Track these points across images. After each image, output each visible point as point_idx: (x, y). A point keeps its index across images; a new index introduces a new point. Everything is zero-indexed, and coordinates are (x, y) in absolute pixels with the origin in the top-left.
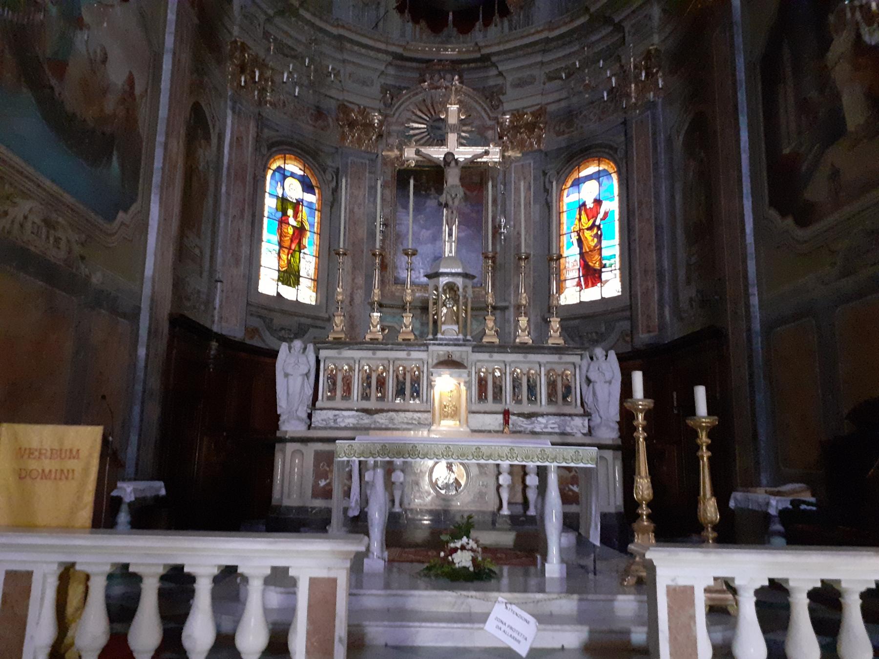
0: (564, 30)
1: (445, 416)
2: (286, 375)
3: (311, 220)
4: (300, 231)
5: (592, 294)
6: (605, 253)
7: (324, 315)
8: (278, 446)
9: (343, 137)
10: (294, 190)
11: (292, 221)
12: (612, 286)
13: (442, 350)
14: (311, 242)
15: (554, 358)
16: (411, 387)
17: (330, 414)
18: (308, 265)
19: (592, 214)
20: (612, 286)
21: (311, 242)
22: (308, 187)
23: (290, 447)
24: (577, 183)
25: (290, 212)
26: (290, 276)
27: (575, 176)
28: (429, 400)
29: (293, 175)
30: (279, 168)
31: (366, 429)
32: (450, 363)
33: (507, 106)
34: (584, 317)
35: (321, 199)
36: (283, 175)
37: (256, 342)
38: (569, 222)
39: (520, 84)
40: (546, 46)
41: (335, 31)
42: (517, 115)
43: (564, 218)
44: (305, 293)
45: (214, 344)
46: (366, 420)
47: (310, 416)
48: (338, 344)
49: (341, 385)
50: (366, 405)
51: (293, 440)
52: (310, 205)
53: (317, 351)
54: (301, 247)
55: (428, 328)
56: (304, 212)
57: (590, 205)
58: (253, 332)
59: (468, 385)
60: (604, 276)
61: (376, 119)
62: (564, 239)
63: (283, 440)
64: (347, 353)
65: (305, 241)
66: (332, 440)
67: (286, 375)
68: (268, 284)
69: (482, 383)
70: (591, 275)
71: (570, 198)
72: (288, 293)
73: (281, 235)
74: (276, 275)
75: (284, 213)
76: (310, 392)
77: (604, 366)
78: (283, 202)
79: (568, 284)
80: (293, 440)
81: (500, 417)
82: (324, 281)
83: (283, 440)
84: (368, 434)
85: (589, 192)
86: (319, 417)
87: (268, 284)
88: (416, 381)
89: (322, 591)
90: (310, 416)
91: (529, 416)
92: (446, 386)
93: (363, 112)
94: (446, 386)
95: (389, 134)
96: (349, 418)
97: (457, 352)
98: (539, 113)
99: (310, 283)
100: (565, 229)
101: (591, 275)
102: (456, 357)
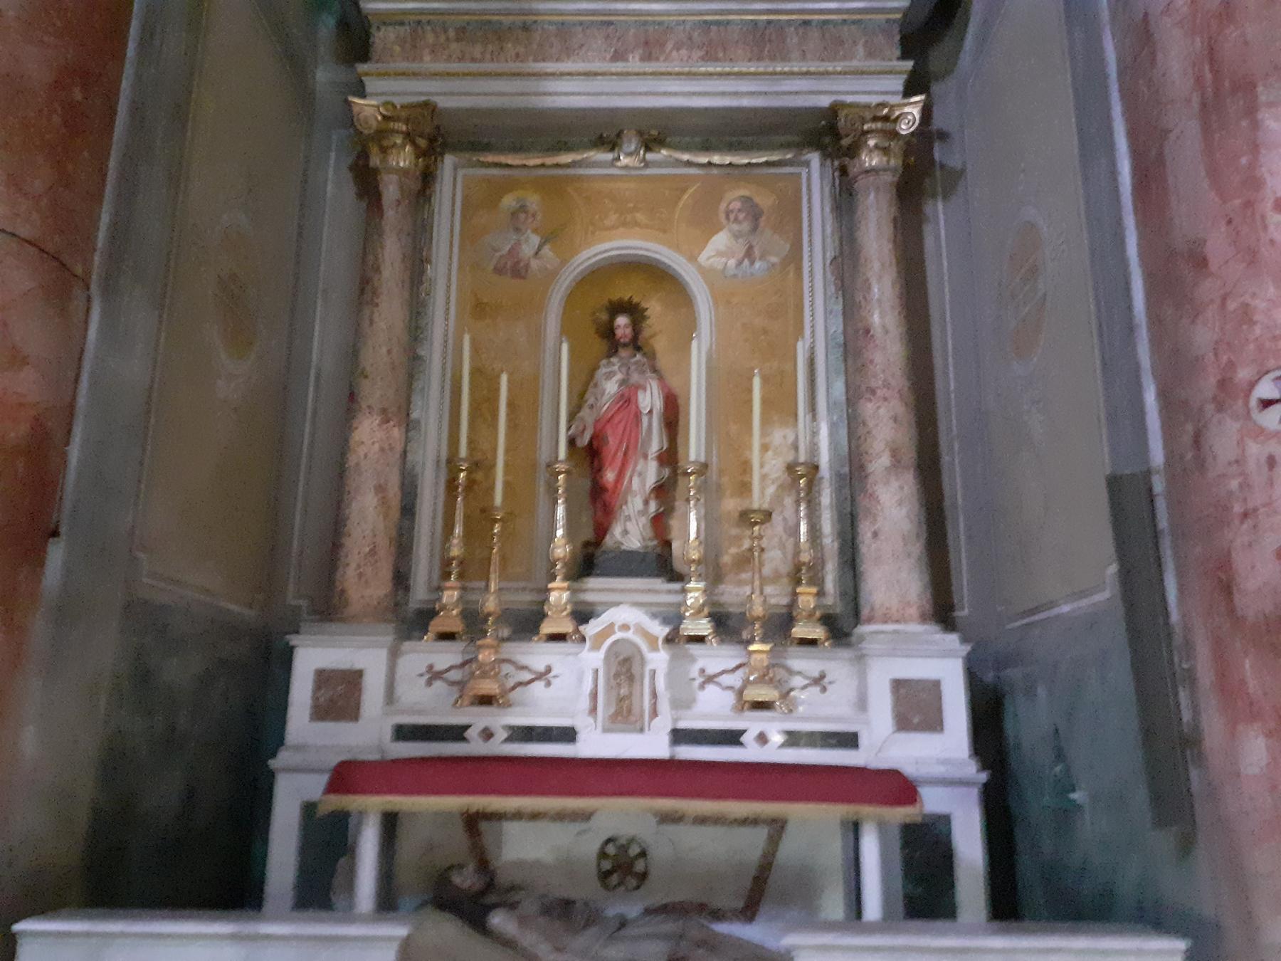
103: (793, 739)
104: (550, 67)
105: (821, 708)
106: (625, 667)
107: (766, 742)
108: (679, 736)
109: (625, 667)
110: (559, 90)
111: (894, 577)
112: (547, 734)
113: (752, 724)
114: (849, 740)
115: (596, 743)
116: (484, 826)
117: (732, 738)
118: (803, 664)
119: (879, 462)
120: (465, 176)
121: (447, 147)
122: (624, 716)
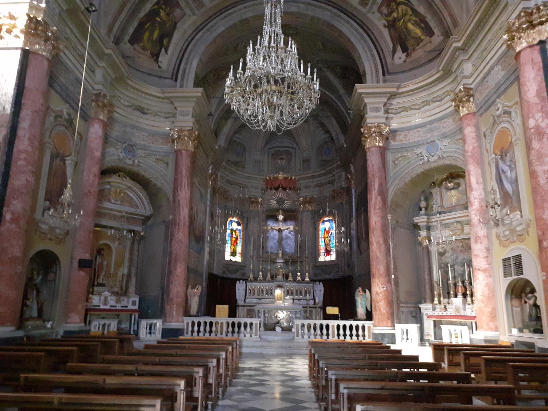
0: (318, 173)
1: (278, 300)
2: (239, 289)
3: (240, 235)
4: (237, 239)
5: (328, 258)
6: (331, 246)
7: (244, 265)
8: (237, 308)
9: (250, 207)
10: (235, 226)
11: (234, 236)
12: (333, 257)
13: (277, 283)
14: (240, 242)
15: (306, 285)
16: (270, 292)
17: (250, 299)
18: (239, 249)
19: (328, 232)
20: (333, 257)
21: (240, 242)
22: (239, 224)
23: (240, 308)
24: (324, 222)
25: (234, 233)
26: (234, 254)
27: (323, 219)
28: (274, 296)
29: (235, 221)
30: (231, 220)
31: (259, 303)
32: (280, 286)
33: (302, 195)
34: (326, 266)
35: (243, 228)
36: (231, 222)
37: (225, 276)
38: (321, 234)
39: (307, 187)
40: (314, 177)
41: (247, 175)
42: (305, 198)
43: (320, 232)
44: (238, 259)
45: (219, 280)
46: (259, 301)
47: (245, 300)
48: (251, 281)
49: (253, 292)
50: (259, 297)
51: (241, 306)
52: (239, 230)
53: (246, 283)
54: (237, 243)
55: (273, 278)
56: (238, 232)
57: (327, 230)
58: (224, 272)
59: (284, 292)
60: (331, 253)
61: (260, 200)
62: (320, 239)
63: (239, 306)
64: (254, 284)
65: (238, 242)
66: (254, 306)
67: (239, 289)
68: (228, 257)
69: (288, 291)
70: (328, 253)
71: (322, 227)
72: (233, 259)
73: (231, 241)
74: (230, 254)
75: (232, 234)
76: (244, 294)
77: (319, 286)
78: (232, 230)
79: (321, 254)
80: (241, 306)
81: (292, 300)
82: (244, 254)
83: (239, 306)
84: (485, 337)
85: (327, 225)
86: (247, 300)
87: (228, 257)
88: (271, 290)
89: (256, 324)
90: (245, 300)
91: (299, 300)
92: (278, 292)
93: (256, 198)
94: (278, 292)
95: (264, 204)
96: (255, 301)
97: (281, 283)
98: (312, 198)
99: (240, 255)
100: (320, 236)
101: (328, 253)
102: (281, 285)
103: (122, 307)
104: (123, 91)
105: (124, 303)
106: (106, 298)
107: (119, 307)
108: (111, 306)
109: (106, 298)
110: (492, 168)
111: (132, 289)
112: (96, 306)
113: (117, 305)
114: (127, 307)
115: (102, 307)
116: (31, 56)
117: (116, 306)
118: (122, 298)
119: (133, 275)
120: (115, 342)
121: (441, 323)
122: (105, 304)
